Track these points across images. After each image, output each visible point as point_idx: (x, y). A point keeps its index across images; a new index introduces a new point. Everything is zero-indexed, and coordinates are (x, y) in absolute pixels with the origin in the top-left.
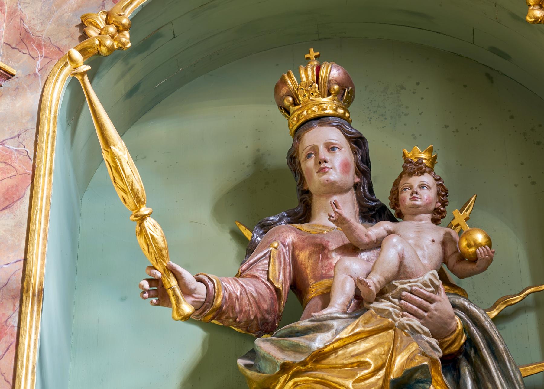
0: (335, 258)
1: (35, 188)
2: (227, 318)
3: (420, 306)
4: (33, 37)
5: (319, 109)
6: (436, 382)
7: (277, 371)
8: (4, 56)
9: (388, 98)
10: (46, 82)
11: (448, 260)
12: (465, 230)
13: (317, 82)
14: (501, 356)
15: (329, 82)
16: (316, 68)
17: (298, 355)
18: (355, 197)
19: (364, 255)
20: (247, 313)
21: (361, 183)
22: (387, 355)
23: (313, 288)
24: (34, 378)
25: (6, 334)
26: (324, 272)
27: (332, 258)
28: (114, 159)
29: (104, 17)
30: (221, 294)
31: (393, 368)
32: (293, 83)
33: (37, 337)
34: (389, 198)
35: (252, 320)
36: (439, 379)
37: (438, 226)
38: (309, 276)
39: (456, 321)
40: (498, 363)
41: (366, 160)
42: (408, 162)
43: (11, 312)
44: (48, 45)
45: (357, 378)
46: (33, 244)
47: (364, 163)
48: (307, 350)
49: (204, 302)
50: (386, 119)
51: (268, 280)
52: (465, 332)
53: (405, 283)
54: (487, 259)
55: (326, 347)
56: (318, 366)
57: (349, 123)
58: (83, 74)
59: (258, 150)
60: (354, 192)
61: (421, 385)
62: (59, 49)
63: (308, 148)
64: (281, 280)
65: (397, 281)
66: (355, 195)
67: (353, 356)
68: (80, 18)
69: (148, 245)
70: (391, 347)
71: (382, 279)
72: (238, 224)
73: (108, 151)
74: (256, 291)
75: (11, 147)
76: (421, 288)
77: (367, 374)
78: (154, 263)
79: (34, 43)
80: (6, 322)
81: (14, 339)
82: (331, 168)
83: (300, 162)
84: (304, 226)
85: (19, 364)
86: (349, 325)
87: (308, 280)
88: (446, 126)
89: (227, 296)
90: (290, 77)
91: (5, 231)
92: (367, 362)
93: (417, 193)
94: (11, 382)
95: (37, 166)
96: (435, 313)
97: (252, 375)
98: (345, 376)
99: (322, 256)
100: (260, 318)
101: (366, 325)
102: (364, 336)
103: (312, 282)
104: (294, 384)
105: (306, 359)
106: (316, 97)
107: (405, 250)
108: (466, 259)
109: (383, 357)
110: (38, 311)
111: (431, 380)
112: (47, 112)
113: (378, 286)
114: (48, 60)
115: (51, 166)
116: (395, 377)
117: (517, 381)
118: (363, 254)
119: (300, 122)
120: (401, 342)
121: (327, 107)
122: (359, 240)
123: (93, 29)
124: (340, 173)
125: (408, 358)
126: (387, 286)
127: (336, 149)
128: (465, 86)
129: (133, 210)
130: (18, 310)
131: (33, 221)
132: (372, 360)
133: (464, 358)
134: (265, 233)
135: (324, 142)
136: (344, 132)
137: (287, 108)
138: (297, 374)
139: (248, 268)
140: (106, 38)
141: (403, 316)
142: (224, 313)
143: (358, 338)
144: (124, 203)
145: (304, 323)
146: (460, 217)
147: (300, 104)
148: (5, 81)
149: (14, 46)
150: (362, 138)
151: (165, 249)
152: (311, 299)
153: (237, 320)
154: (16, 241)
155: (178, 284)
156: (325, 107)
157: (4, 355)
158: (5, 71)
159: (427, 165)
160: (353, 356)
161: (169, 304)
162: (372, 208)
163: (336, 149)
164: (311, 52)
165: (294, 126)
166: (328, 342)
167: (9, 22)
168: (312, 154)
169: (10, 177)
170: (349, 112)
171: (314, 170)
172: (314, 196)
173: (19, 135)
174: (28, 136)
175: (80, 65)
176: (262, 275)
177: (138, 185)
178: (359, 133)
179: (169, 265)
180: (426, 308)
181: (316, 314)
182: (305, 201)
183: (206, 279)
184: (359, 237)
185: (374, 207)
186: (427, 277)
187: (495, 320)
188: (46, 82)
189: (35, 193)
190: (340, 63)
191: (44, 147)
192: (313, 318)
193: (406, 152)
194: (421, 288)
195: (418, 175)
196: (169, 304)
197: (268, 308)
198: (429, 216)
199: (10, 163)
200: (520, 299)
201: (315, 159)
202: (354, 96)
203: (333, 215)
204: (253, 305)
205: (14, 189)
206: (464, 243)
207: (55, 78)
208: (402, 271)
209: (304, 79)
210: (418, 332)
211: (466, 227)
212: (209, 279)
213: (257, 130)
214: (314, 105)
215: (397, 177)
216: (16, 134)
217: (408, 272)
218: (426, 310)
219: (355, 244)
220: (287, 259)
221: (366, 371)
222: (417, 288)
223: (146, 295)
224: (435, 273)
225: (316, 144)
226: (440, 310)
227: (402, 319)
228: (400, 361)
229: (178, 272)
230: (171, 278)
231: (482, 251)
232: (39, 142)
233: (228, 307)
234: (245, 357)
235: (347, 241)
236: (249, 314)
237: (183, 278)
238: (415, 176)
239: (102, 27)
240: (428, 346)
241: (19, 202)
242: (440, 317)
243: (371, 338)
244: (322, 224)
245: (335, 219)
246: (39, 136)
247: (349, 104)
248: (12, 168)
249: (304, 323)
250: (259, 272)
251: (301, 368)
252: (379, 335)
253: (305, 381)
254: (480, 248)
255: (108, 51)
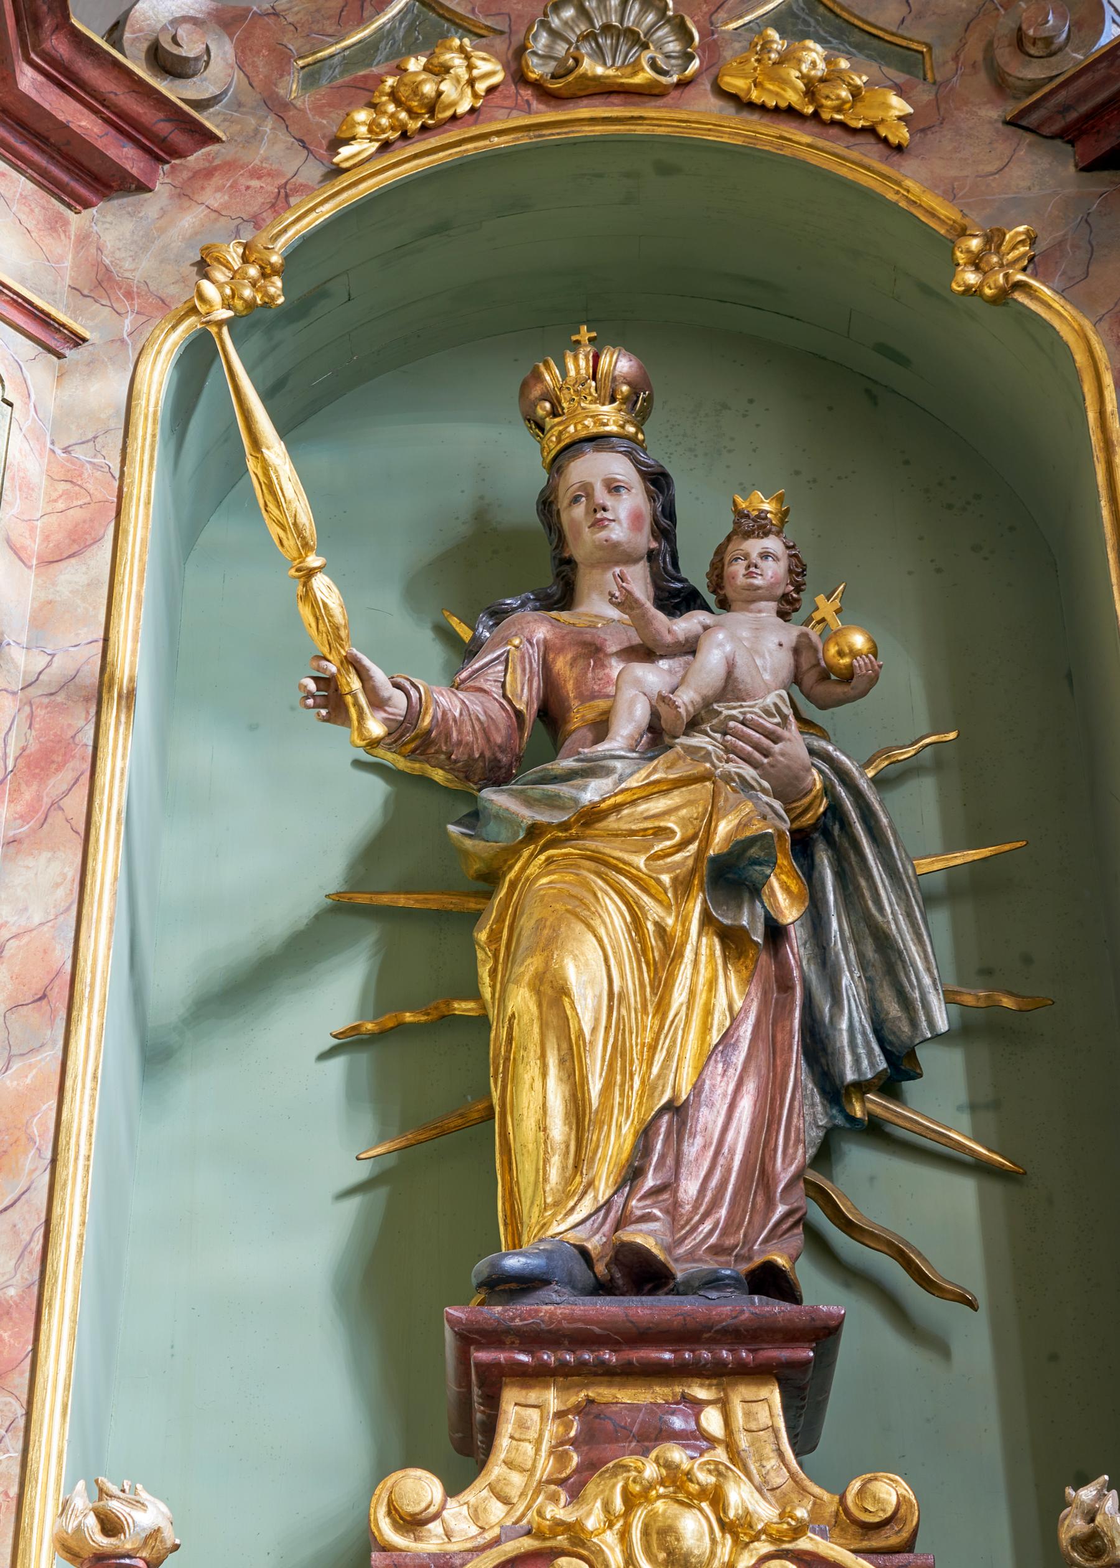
0: (616, 667)
1: (123, 524)
2: (436, 752)
3: (757, 747)
4: (117, 278)
5: (595, 423)
6: (781, 868)
7: (520, 838)
8: (69, 308)
9: (701, 421)
10: (140, 354)
11: (801, 679)
12: (834, 628)
13: (594, 378)
14: (883, 834)
15: (614, 379)
16: (593, 356)
17: (556, 813)
18: (648, 574)
19: (664, 664)
20: (469, 746)
21: (659, 550)
22: (702, 821)
23: (578, 712)
24: (120, 828)
25: (73, 757)
26: (596, 688)
27: (611, 666)
28: (268, 471)
29: (240, 250)
30: (431, 711)
31: (713, 839)
32: (553, 378)
33: (125, 764)
34: (707, 574)
35: (476, 760)
36: (785, 863)
37: (787, 623)
38: (571, 695)
39: (812, 775)
40: (878, 847)
41: (669, 513)
42: (741, 514)
43: (82, 723)
44: (143, 293)
45: (652, 852)
46: (120, 616)
47: (665, 517)
48: (572, 804)
49: (403, 722)
50: (696, 456)
51: (504, 696)
52: (826, 795)
53: (734, 708)
54: (869, 676)
55: (604, 800)
56: (588, 832)
57: (644, 450)
58: (220, 324)
59: (482, 498)
60: (647, 564)
61: (758, 868)
62: (163, 301)
63: (575, 486)
64: (525, 698)
65: (721, 704)
66: (648, 569)
67: (646, 818)
68: (198, 252)
69: (317, 620)
70: (707, 809)
71: (697, 698)
72: (447, 614)
73: (257, 458)
74: (485, 712)
75: (81, 457)
76: (760, 717)
77: (670, 848)
78: (325, 650)
79: (120, 288)
80: (73, 737)
81: (87, 766)
82: (614, 521)
83: (558, 511)
84: (564, 616)
85: (96, 805)
86: (640, 769)
87: (568, 701)
88: (797, 473)
89: (439, 715)
90: (548, 367)
91: (71, 592)
92: (669, 828)
93: (756, 567)
94: (82, 834)
95: (125, 489)
96: (782, 759)
97: (474, 846)
98: (634, 850)
99: (595, 662)
100: (489, 758)
101: (670, 771)
102: (665, 788)
103: (575, 704)
104: (546, 860)
105: (570, 818)
106: (590, 403)
107: (737, 653)
108: (833, 677)
109: (695, 822)
110: (127, 723)
111: (774, 860)
112: (143, 403)
113: (691, 708)
114: (144, 318)
115: (149, 492)
116: (716, 852)
117: (908, 877)
118: (661, 662)
119: (562, 444)
120: (726, 800)
121: (608, 420)
122: (658, 638)
123: (221, 270)
124: (629, 528)
125: (739, 823)
126: (703, 712)
127: (622, 489)
128: (830, 409)
129: (295, 559)
130: (94, 720)
131: (120, 578)
132: (678, 826)
133: (822, 837)
134: (496, 624)
135: (603, 477)
136: (636, 462)
137: (540, 422)
138: (553, 843)
139: (470, 677)
140: (244, 285)
141: (727, 761)
142: (433, 743)
143: (656, 790)
144: (280, 548)
145: (567, 763)
146: (826, 608)
147: (564, 414)
148: (71, 349)
149: (86, 292)
150: (665, 475)
151: (345, 626)
152: (574, 731)
153: (453, 757)
154: (91, 609)
155: (363, 687)
156: (605, 421)
157: (70, 790)
158: (71, 332)
159: (774, 522)
160: (646, 818)
161: (346, 720)
162: (676, 593)
163: (622, 489)
164: (582, 332)
165: (550, 451)
166: (608, 793)
167: (78, 253)
168: (582, 496)
169: (81, 506)
170: (643, 433)
171: (584, 523)
172: (582, 569)
173: (95, 438)
174: (110, 441)
175: (216, 308)
176: (494, 689)
177: (306, 518)
178: (661, 466)
179: (351, 654)
180: (766, 750)
181: (586, 750)
182: (564, 577)
183: (407, 685)
184: (658, 632)
185: (679, 590)
186: (770, 700)
187: (875, 781)
188: (140, 354)
189: (123, 533)
190: (631, 350)
191: (138, 458)
192: (582, 756)
193: (739, 500)
194: (760, 717)
195: (758, 537)
196: (346, 720)
197: (502, 742)
198: (773, 605)
199: (79, 483)
200: (913, 753)
201: (587, 504)
202: (652, 407)
203: (617, 594)
204: (480, 735)
205: (86, 526)
206: (833, 650)
207: (156, 347)
208: (730, 688)
209: (572, 373)
210: (753, 788)
211: (836, 623)
212: (413, 684)
213: (480, 464)
214: (587, 416)
215: (722, 540)
216: (90, 436)
217: (740, 690)
218: (766, 753)
219: (650, 644)
220: (535, 665)
221: (668, 843)
222: (754, 716)
223: (310, 702)
224: (784, 693)
225: (589, 480)
226: (789, 754)
227: (726, 766)
228: (725, 828)
229: (364, 667)
230: (351, 676)
231: (862, 662)
232: (129, 450)
233: (440, 733)
234: (458, 823)
235: (636, 640)
236: (472, 749)
237: (371, 678)
238: (754, 538)
239: (236, 268)
240: (768, 809)
241: (95, 546)
242: (788, 767)
243: (676, 792)
244: (594, 612)
245: (619, 600)
246: (129, 441)
247: (644, 419)
248: (83, 491)
249: (567, 763)
250: (489, 683)
251: (560, 834)
252: (690, 788)
253: (566, 854)
254: (858, 658)
255: (246, 308)
